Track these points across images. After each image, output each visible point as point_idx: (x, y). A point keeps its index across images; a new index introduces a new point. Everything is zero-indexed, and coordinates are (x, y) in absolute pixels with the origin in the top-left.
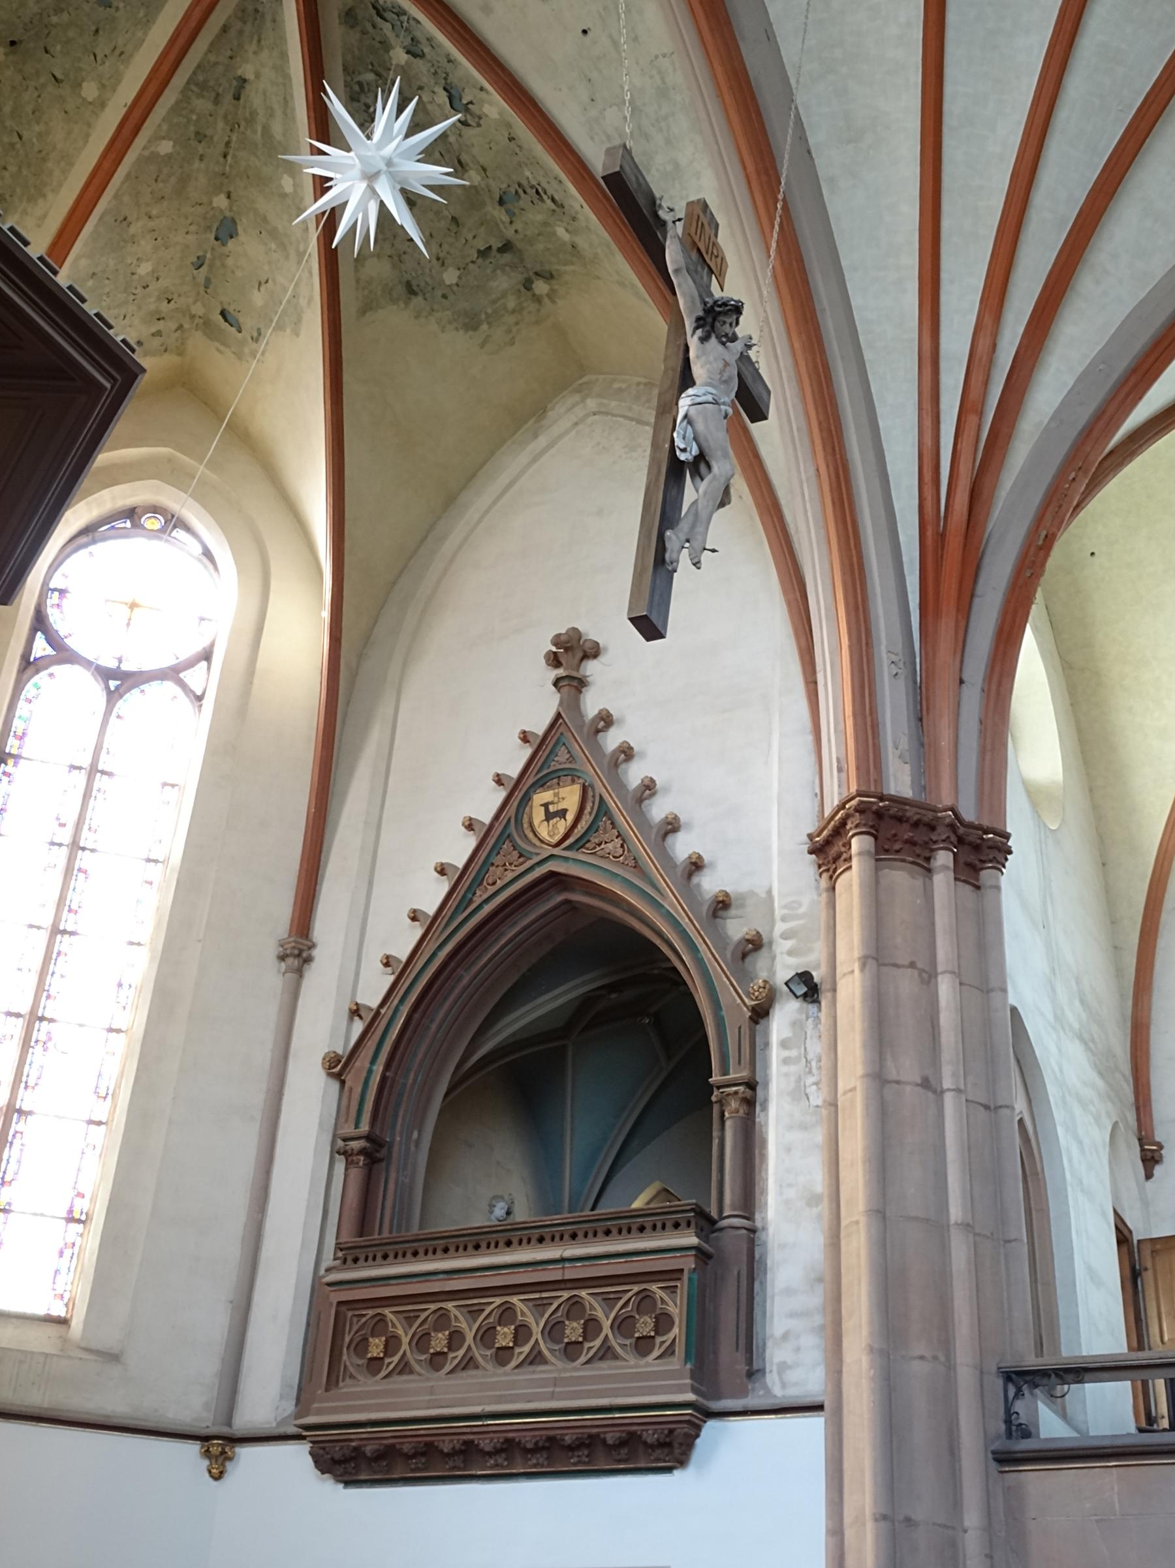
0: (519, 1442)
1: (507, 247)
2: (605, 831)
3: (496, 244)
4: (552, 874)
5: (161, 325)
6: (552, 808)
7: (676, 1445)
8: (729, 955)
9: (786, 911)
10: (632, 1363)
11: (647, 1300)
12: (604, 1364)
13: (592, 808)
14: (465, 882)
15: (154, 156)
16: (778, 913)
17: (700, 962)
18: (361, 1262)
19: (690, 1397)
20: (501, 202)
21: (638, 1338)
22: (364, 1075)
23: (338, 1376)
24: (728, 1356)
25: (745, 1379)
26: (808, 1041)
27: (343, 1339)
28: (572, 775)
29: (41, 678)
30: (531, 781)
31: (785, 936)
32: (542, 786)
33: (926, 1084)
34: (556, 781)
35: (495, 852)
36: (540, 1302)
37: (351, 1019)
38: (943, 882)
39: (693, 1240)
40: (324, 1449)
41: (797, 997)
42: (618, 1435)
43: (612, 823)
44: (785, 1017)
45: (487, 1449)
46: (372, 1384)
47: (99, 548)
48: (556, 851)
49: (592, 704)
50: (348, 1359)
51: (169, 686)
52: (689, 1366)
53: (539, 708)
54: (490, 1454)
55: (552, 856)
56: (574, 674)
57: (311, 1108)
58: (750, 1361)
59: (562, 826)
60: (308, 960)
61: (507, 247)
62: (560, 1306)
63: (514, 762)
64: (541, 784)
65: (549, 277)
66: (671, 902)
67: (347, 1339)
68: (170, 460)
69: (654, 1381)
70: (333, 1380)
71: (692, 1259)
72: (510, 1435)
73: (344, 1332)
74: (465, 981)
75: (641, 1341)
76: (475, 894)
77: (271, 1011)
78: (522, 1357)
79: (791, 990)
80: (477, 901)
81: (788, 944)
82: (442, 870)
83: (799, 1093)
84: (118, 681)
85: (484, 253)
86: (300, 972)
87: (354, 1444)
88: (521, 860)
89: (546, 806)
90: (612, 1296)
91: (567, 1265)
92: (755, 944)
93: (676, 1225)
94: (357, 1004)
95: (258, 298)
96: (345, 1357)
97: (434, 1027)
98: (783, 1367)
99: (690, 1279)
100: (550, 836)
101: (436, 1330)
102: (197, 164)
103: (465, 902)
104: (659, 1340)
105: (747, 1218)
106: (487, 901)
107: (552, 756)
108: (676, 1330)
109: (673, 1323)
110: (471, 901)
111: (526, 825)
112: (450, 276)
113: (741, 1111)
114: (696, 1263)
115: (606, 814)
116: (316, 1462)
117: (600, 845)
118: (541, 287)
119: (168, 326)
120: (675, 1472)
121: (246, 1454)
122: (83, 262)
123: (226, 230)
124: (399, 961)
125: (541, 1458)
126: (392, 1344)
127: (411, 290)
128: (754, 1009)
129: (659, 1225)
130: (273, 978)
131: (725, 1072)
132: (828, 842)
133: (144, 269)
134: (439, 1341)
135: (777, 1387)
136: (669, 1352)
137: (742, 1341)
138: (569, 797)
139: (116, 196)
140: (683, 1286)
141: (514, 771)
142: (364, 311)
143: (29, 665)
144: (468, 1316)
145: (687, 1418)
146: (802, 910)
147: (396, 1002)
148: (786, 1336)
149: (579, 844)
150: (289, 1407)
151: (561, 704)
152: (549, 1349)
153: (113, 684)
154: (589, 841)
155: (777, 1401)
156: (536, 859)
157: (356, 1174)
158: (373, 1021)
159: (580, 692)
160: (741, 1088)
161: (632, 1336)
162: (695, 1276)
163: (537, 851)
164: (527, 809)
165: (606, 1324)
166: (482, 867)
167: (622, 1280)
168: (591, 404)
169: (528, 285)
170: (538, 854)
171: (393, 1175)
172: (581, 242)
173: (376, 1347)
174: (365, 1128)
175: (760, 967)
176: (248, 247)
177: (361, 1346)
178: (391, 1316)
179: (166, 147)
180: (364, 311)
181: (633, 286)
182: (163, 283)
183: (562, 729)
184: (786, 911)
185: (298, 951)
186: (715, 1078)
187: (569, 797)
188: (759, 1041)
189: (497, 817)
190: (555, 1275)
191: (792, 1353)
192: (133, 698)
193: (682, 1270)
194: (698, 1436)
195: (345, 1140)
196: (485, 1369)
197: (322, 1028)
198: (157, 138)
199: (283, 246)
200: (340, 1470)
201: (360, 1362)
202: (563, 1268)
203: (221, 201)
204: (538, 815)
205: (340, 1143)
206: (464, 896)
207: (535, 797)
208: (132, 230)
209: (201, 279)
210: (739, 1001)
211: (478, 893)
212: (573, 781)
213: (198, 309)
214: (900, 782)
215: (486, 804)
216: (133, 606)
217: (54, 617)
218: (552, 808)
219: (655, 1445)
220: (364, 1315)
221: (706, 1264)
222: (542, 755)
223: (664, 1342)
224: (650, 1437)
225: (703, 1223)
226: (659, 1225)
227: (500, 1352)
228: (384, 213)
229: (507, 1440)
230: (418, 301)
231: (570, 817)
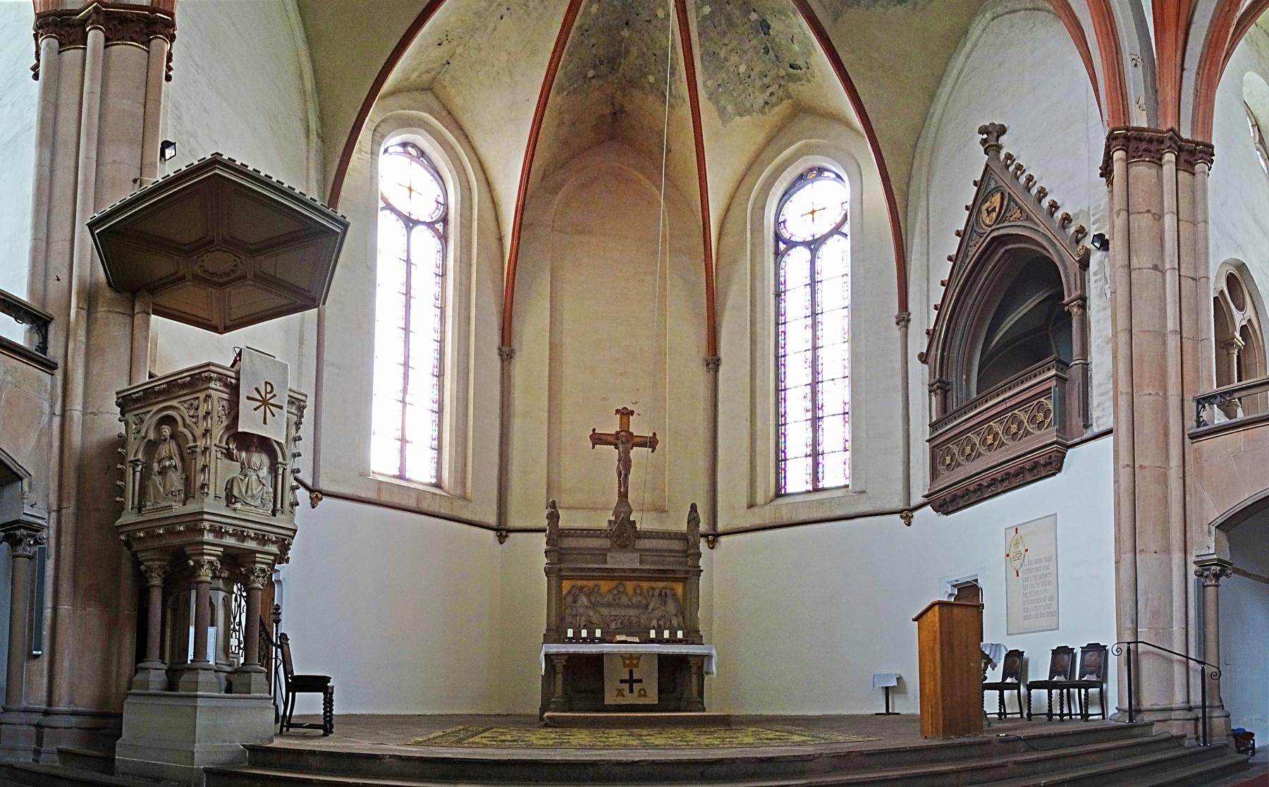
5: (771, 90)
15: (705, 18)
17: (1057, 251)
28: (997, 189)
29: (786, 258)
33: (1155, 268)
47: (794, 198)
50: (941, 468)
51: (836, 237)
57: (920, 375)
59: (994, 215)
60: (909, 321)
64: (985, 201)
68: (806, 145)
84: (814, 245)
86: (906, 327)
102: (728, 8)
119: (774, 88)
121: (723, 539)
122: (709, 83)
123: (765, 27)
128: (1079, 261)
130: (897, 332)
133: (742, 69)
139: (701, 46)
143: (778, 254)
153: (782, 246)
176: (776, 25)
179: (707, 10)
180: (836, 17)
182: (757, 70)
185: (904, 319)
192: (824, 250)
197: (918, 343)
198: (698, 9)
199: (786, 15)
203: (754, 16)
208: (722, 55)
209: (774, 58)
213: (782, 73)
216: (813, 212)
217: (786, 235)
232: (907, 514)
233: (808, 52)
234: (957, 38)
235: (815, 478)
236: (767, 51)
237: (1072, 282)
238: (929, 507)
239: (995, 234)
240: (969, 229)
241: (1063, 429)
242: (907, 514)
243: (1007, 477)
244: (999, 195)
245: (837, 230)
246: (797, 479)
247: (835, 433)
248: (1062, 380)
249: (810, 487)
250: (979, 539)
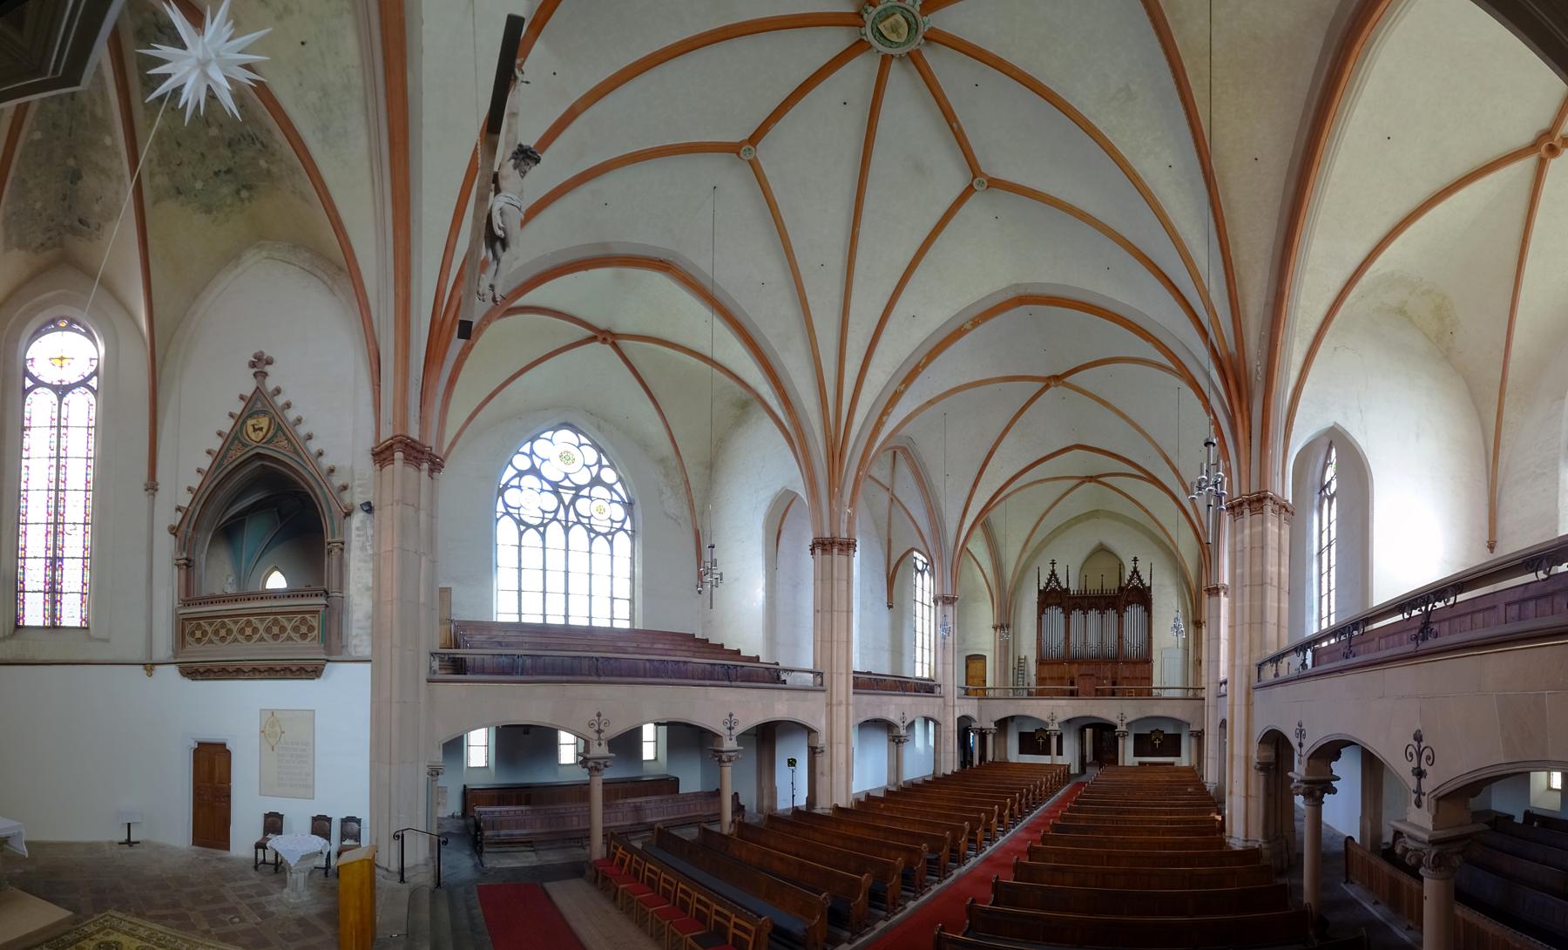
1: (229, 171)
3: (223, 168)
14: (219, 457)
20: (230, 145)
29: (31, 395)
38: (425, 474)
44: (358, 518)
46: (199, 647)
49: (270, 384)
51: (83, 389)
57: (166, 547)
59: (261, 434)
61: (229, 171)
63: (238, 407)
64: (250, 416)
65: (249, 188)
69: (306, 649)
70: (183, 646)
73: (186, 629)
82: (209, 452)
83: (363, 548)
84: (62, 390)
85: (217, 174)
95: (97, 208)
103: (220, 465)
112: (199, 185)
118: (244, 194)
123: (76, 176)
127: (179, 192)
130: (144, 497)
132: (382, 452)
133: (38, 205)
138: (264, 422)
141: (238, 411)
142: (155, 203)
149: (269, 442)
157: (183, 572)
168: (264, 254)
169: (238, 192)
172: (274, 169)
173: (198, 634)
175: (347, 497)
179: (37, 135)
180: (155, 203)
181: (509, 131)
185: (152, 487)
187: (264, 422)
191: (358, 635)
192: (69, 397)
197: (167, 516)
203: (71, 162)
204: (250, 429)
213: (67, 222)
214: (414, 434)
215: (227, 425)
219: (310, 671)
228: (212, 96)
230: (182, 197)
232: (149, 666)
233: (110, 214)
234: (231, 258)
235: (53, 616)
236: (64, 199)
242: (149, 666)
245: (84, 383)
246: (34, 613)
247: (73, 576)
249: (48, 623)
250: (238, 710)
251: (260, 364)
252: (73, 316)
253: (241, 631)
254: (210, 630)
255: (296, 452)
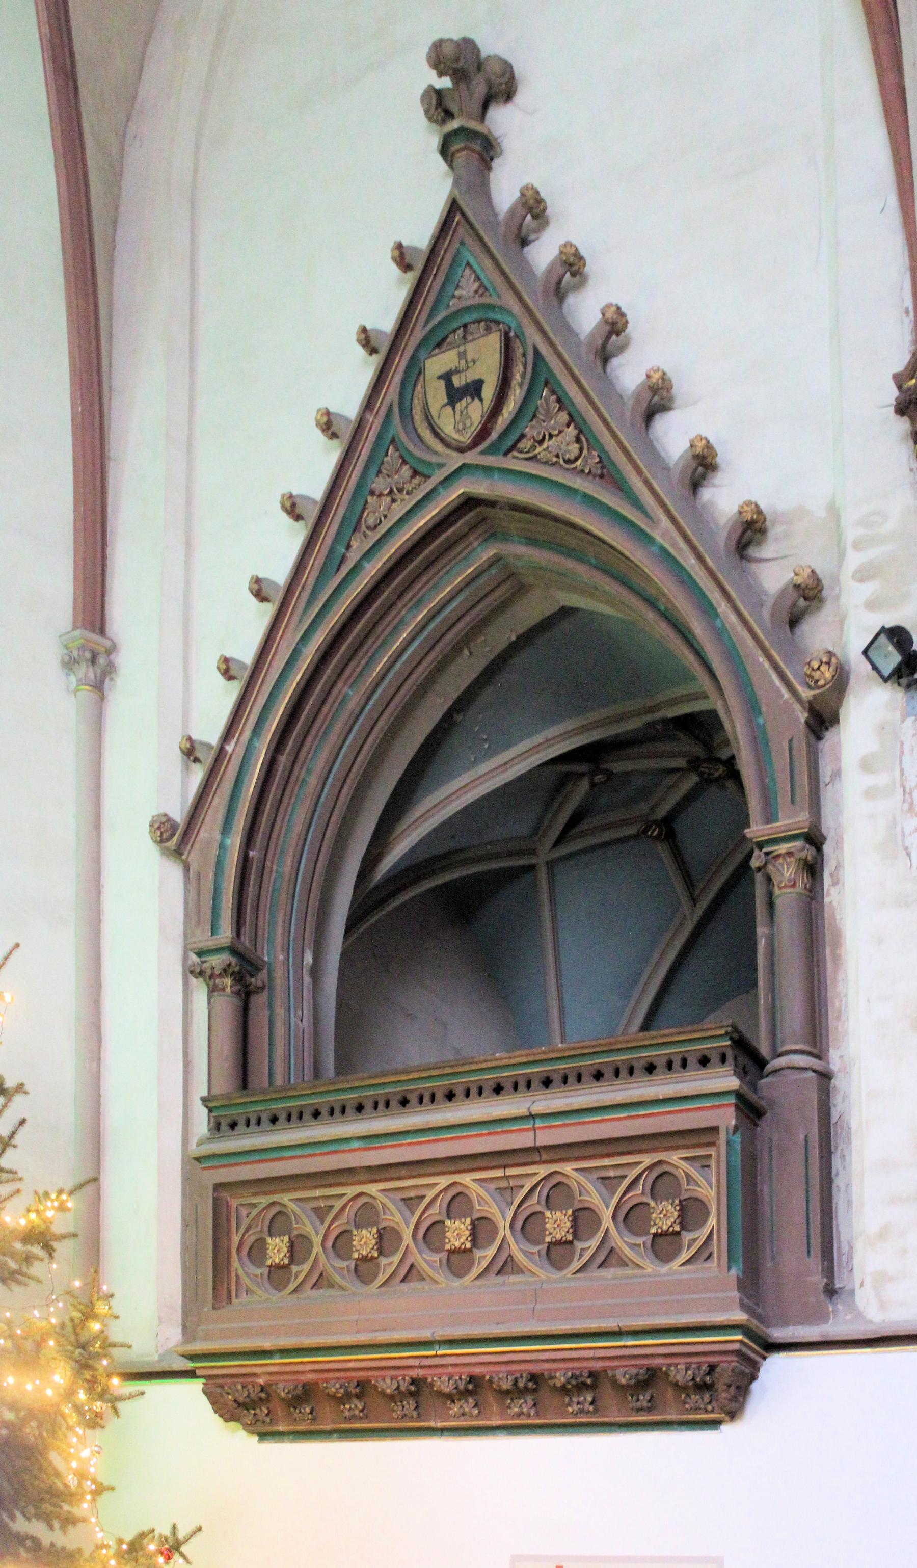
0: (491, 1381)
2: (549, 416)
4: (469, 503)
6: (457, 381)
7: (720, 1386)
8: (766, 613)
9: (861, 531)
10: (650, 1270)
11: (666, 1179)
12: (608, 1273)
13: (523, 376)
14: (328, 521)
16: (851, 534)
18: (241, 1127)
19: (740, 1316)
21: (655, 1235)
22: (215, 851)
23: (229, 1292)
24: (792, 1259)
25: (822, 1297)
26: (906, 757)
27: (229, 1239)
28: (486, 317)
30: (419, 334)
31: (863, 575)
32: (439, 345)
34: (460, 332)
35: (373, 471)
36: (504, 1184)
37: (186, 769)
39: (733, 1083)
40: (222, 1386)
41: (886, 680)
42: (634, 1371)
43: (559, 400)
45: (447, 1388)
48: (471, 457)
49: (505, 189)
52: (734, 1272)
53: (415, 194)
54: (450, 1397)
55: (464, 466)
56: (473, 125)
57: (150, 913)
58: (829, 1271)
59: (476, 411)
60: (110, 670)
62: (533, 1189)
63: (383, 300)
64: (437, 342)
66: (662, 531)
67: (236, 1239)
71: (731, 1111)
72: (477, 1370)
74: (352, 705)
75: (660, 1240)
76: (348, 547)
77: (67, 753)
78: (484, 1264)
79: (875, 668)
80: (353, 557)
81: (868, 589)
86: (99, 687)
87: (261, 1381)
88: (416, 481)
89: (447, 377)
90: (612, 1173)
91: (539, 1123)
92: (808, 596)
93: (704, 1061)
94: (190, 739)
96: (235, 1263)
97: (313, 781)
98: (882, 1279)
99: (729, 1143)
100: (458, 431)
101: (358, 1226)
103: (333, 562)
104: (687, 1236)
105: (819, 1057)
106: (369, 554)
107: (450, 289)
108: (712, 1221)
109: (707, 1214)
110: (343, 559)
111: (418, 417)
113: (800, 885)
114: (737, 1118)
115: (546, 383)
116: (213, 1403)
117: (541, 442)
120: (724, 1427)
124: (243, 666)
125: (523, 1405)
126: (298, 1249)
129: (677, 1063)
130: (59, 698)
131: (770, 817)
134: (364, 1241)
135: (873, 1308)
136: (703, 1254)
137: (816, 1241)
138: (484, 358)
140: (718, 1154)
144: (401, 1204)
145: (736, 1346)
146: (890, 526)
147: (247, 733)
148: (883, 1234)
150: (174, 1335)
151: (456, 183)
152: (524, 1252)
154: (523, 436)
155: (872, 1327)
156: (438, 476)
157: (227, 1004)
158: (212, 762)
159: (489, 168)
160: (799, 844)
161: (648, 1233)
162: (737, 1139)
163: (441, 460)
164: (419, 388)
165: (606, 1215)
166: (354, 496)
167: (622, 1147)
170: (441, 466)
171: (280, 1011)
174: (226, 934)
175: (817, 634)
177: (257, 1252)
178: (292, 1206)
183: (462, 232)
184: (861, 531)
185: (92, 647)
186: (756, 830)
188: (826, 771)
189: (369, 404)
190: (523, 1140)
193: (715, 1130)
194: (753, 1378)
195: (200, 954)
196: (436, 1282)
197: (149, 781)
200: (248, 1418)
201: (258, 1271)
202: (534, 1129)
205: (194, 958)
206: (332, 550)
207: (428, 363)
210: (786, 695)
211: (355, 544)
212: (488, 329)
215: (348, 384)
218: (457, 381)
220: (254, 1205)
221: (756, 1125)
222: (434, 285)
223: (695, 1240)
224: (681, 1375)
225: (744, 1060)
226: (677, 1063)
227: (454, 1258)
229: (472, 1379)
231: (488, 393)
237: (782, 778)
238: (195, 1387)
239: (480, 487)
240: (375, 423)
241: (751, 1285)
243: (589, 1383)
244: (494, 341)
248: (750, 1110)
251: (469, 94)
252: (451, 329)
253: (431, 1235)
254: (406, 1226)
255: (606, 473)
